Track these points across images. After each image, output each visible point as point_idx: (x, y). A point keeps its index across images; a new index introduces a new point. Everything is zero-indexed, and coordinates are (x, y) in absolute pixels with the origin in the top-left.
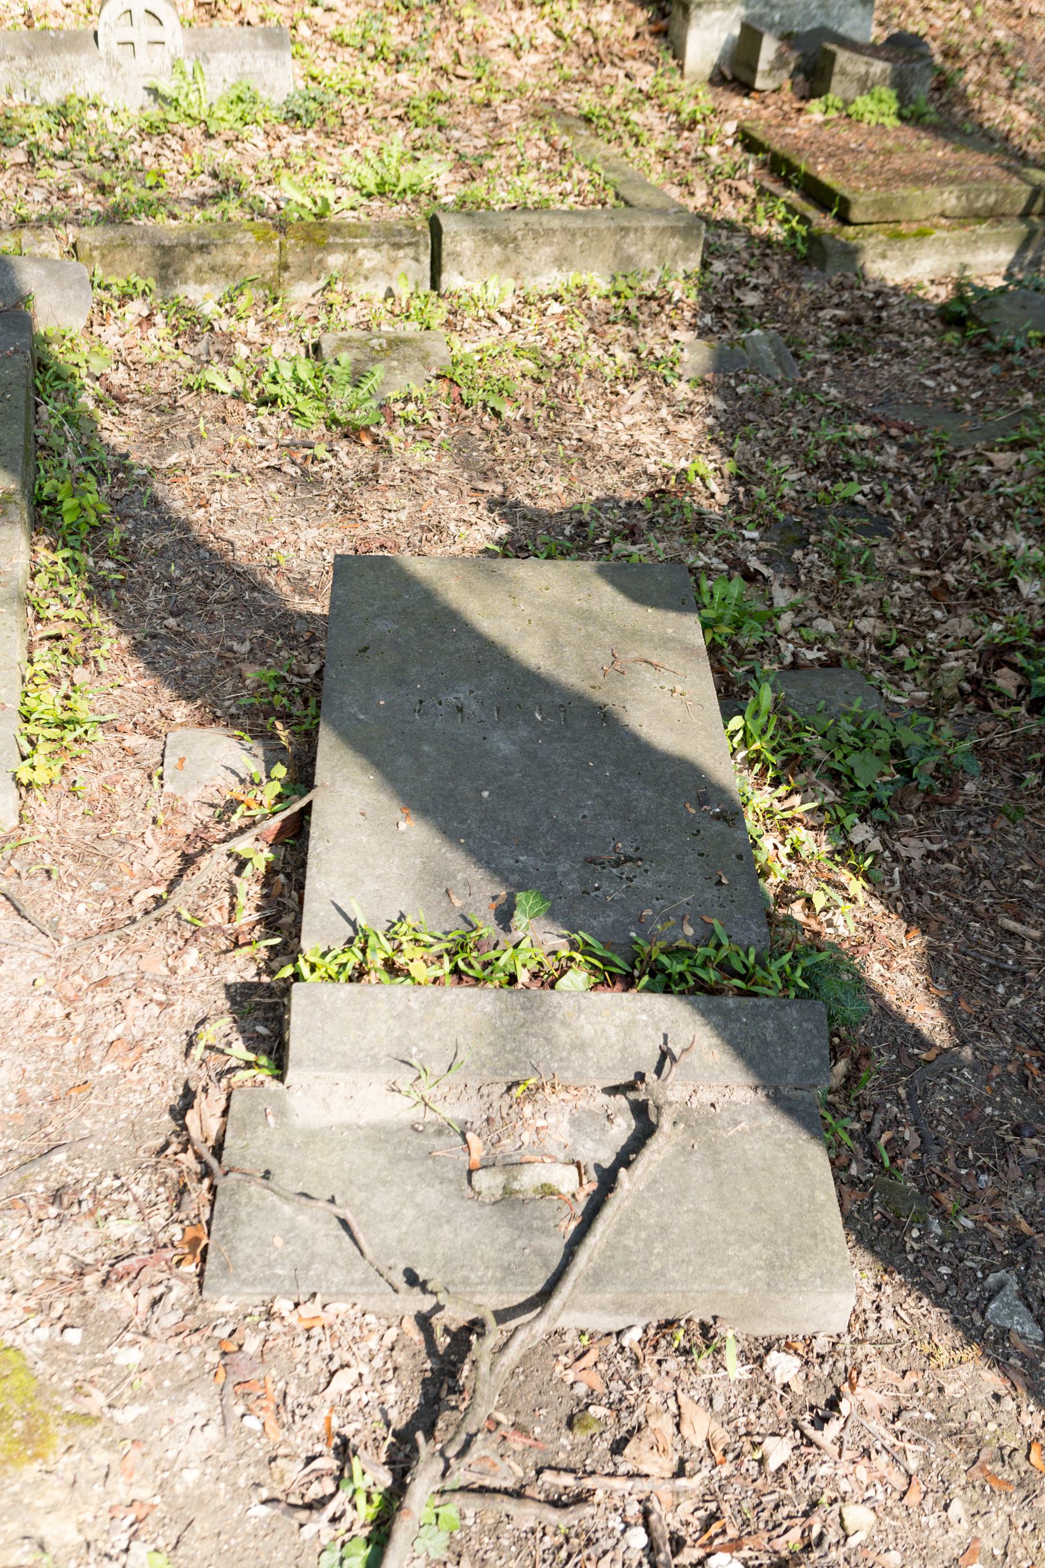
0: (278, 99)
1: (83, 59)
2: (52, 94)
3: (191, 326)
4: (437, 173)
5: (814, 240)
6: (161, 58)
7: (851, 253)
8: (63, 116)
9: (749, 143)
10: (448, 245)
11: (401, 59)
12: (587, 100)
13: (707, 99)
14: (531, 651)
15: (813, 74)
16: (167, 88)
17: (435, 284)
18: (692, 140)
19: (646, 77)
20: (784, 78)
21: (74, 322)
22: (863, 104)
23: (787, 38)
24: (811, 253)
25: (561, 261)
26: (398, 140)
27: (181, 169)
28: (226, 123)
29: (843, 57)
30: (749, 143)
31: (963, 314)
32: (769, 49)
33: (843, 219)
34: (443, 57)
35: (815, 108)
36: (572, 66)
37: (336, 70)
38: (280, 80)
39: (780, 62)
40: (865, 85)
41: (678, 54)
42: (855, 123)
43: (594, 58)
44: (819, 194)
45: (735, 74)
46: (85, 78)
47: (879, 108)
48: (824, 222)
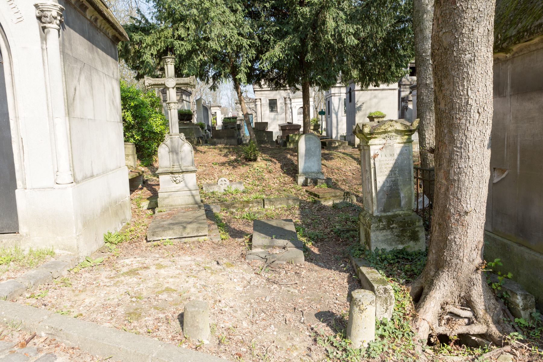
0: (241, 190)
1: (215, 186)
2: (211, 191)
3: (232, 213)
4: (264, 196)
5: (315, 200)
6: (226, 186)
7: (320, 202)
8: (213, 193)
9: (307, 191)
10: (265, 202)
11: (258, 185)
12: (284, 188)
13: (301, 187)
14: (275, 225)
15: (315, 182)
16: (226, 189)
17: (264, 207)
18: (299, 192)
19: (292, 185)
20: (312, 184)
21: (218, 212)
22: (322, 186)
23: (312, 179)
24: (315, 202)
25: (280, 204)
26: (258, 193)
27: (229, 199)
28: (234, 193)
29: (319, 180)
30: (307, 191)
31: (335, 206)
32: (309, 180)
33: (319, 198)
34: (264, 185)
35: (316, 187)
36: (282, 185)
37: (250, 187)
38: (242, 188)
39: (311, 182)
40: (322, 183)
41: (297, 183)
42: (321, 188)
43: (285, 184)
44: (315, 195)
45: (305, 184)
46: (215, 189)
47: (324, 186)
48: (316, 199)
